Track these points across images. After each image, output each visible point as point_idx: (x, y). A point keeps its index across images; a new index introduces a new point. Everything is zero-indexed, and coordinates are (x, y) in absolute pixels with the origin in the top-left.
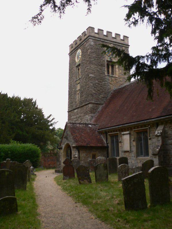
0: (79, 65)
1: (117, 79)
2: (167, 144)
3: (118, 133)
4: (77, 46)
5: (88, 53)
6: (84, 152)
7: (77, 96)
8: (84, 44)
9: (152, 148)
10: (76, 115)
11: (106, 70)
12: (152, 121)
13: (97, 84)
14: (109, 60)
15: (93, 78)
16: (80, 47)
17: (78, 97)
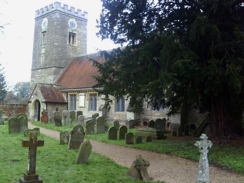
0: (45, 32)
1: (76, 48)
9: (99, 106)
11: (68, 40)
14: (71, 32)
17: (42, 59)
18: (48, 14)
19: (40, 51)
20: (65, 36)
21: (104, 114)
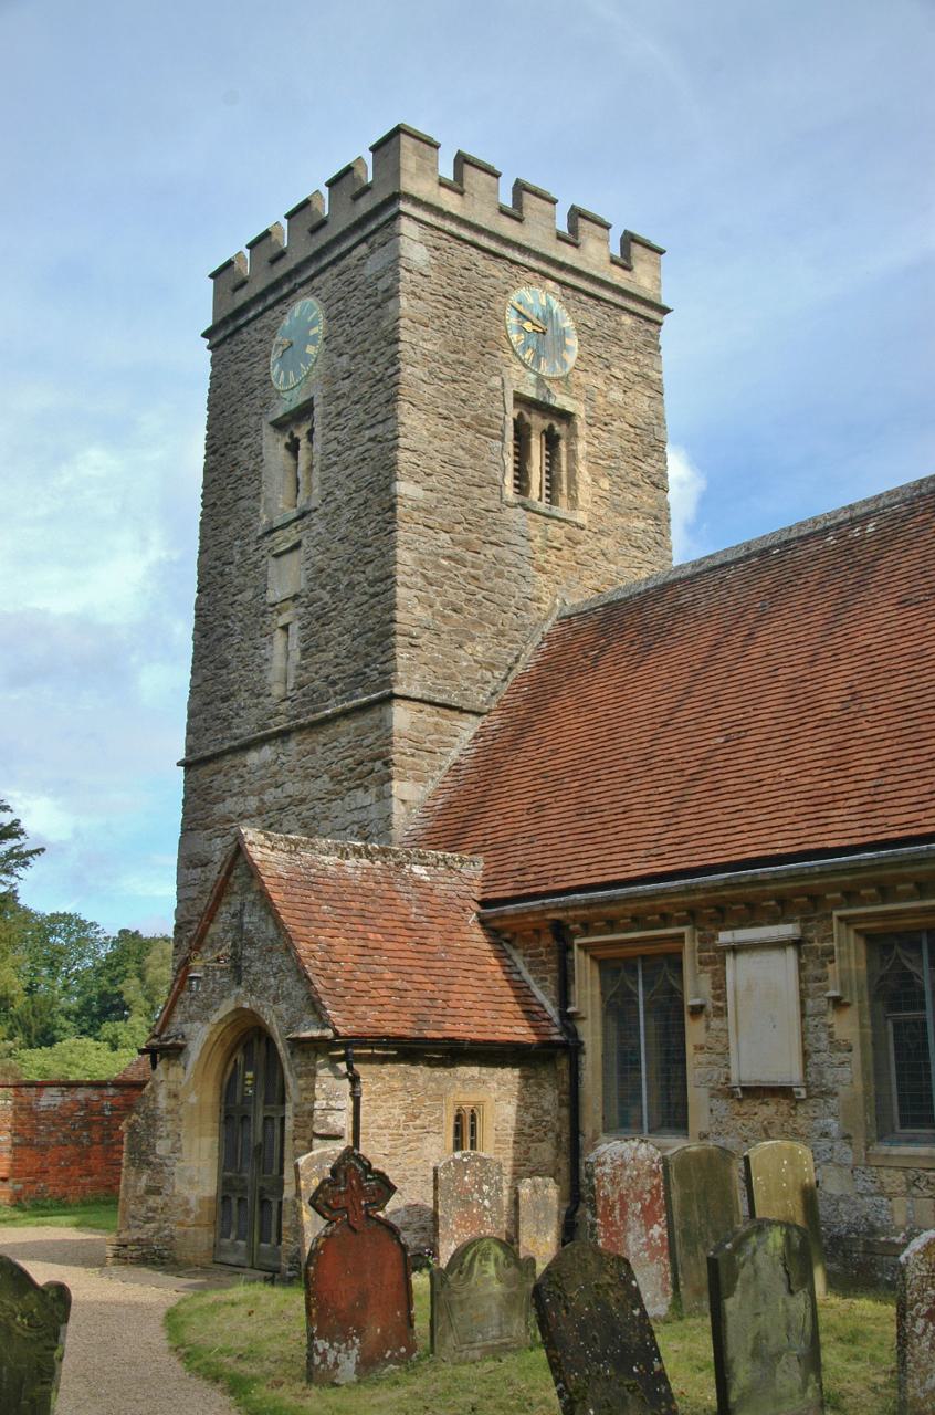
0: (304, 412)
3: (681, 937)
4: (288, 276)
5: (384, 324)
8: (350, 260)
10: (262, 791)
12: (706, 890)
13: (449, 558)
15: (417, 509)
16: (311, 278)
18: (318, 255)
20: (480, 425)
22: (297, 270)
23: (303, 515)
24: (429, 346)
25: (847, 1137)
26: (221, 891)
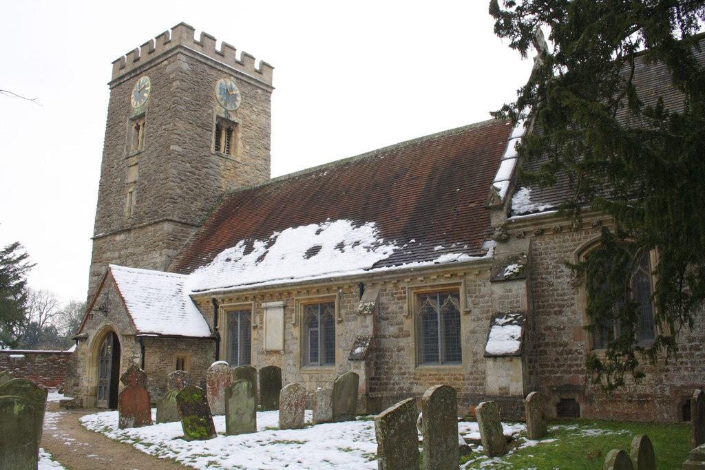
0: (143, 116)
2: (384, 337)
3: (251, 304)
4: (140, 68)
5: (171, 90)
6: (156, 352)
7: (128, 199)
10: (120, 250)
11: (214, 140)
13: (190, 172)
14: (223, 115)
17: (129, 203)
18: (150, 62)
19: (123, 179)
21: (373, 375)
22: (143, 66)
23: (139, 154)
24: (187, 99)
25: (295, 365)
26: (101, 286)
